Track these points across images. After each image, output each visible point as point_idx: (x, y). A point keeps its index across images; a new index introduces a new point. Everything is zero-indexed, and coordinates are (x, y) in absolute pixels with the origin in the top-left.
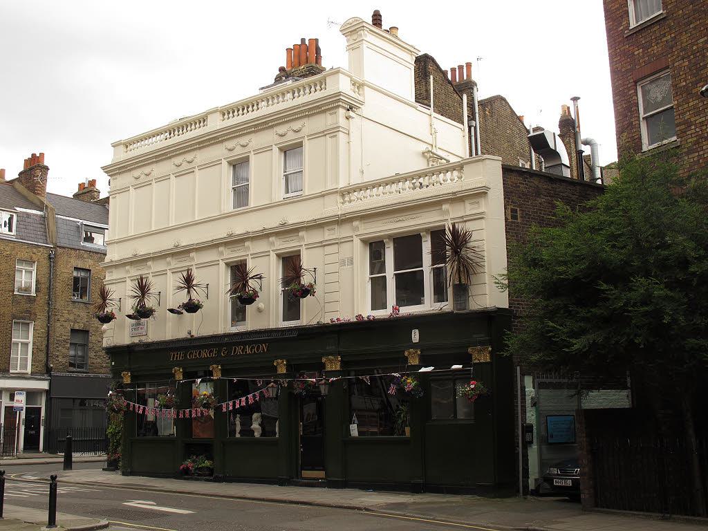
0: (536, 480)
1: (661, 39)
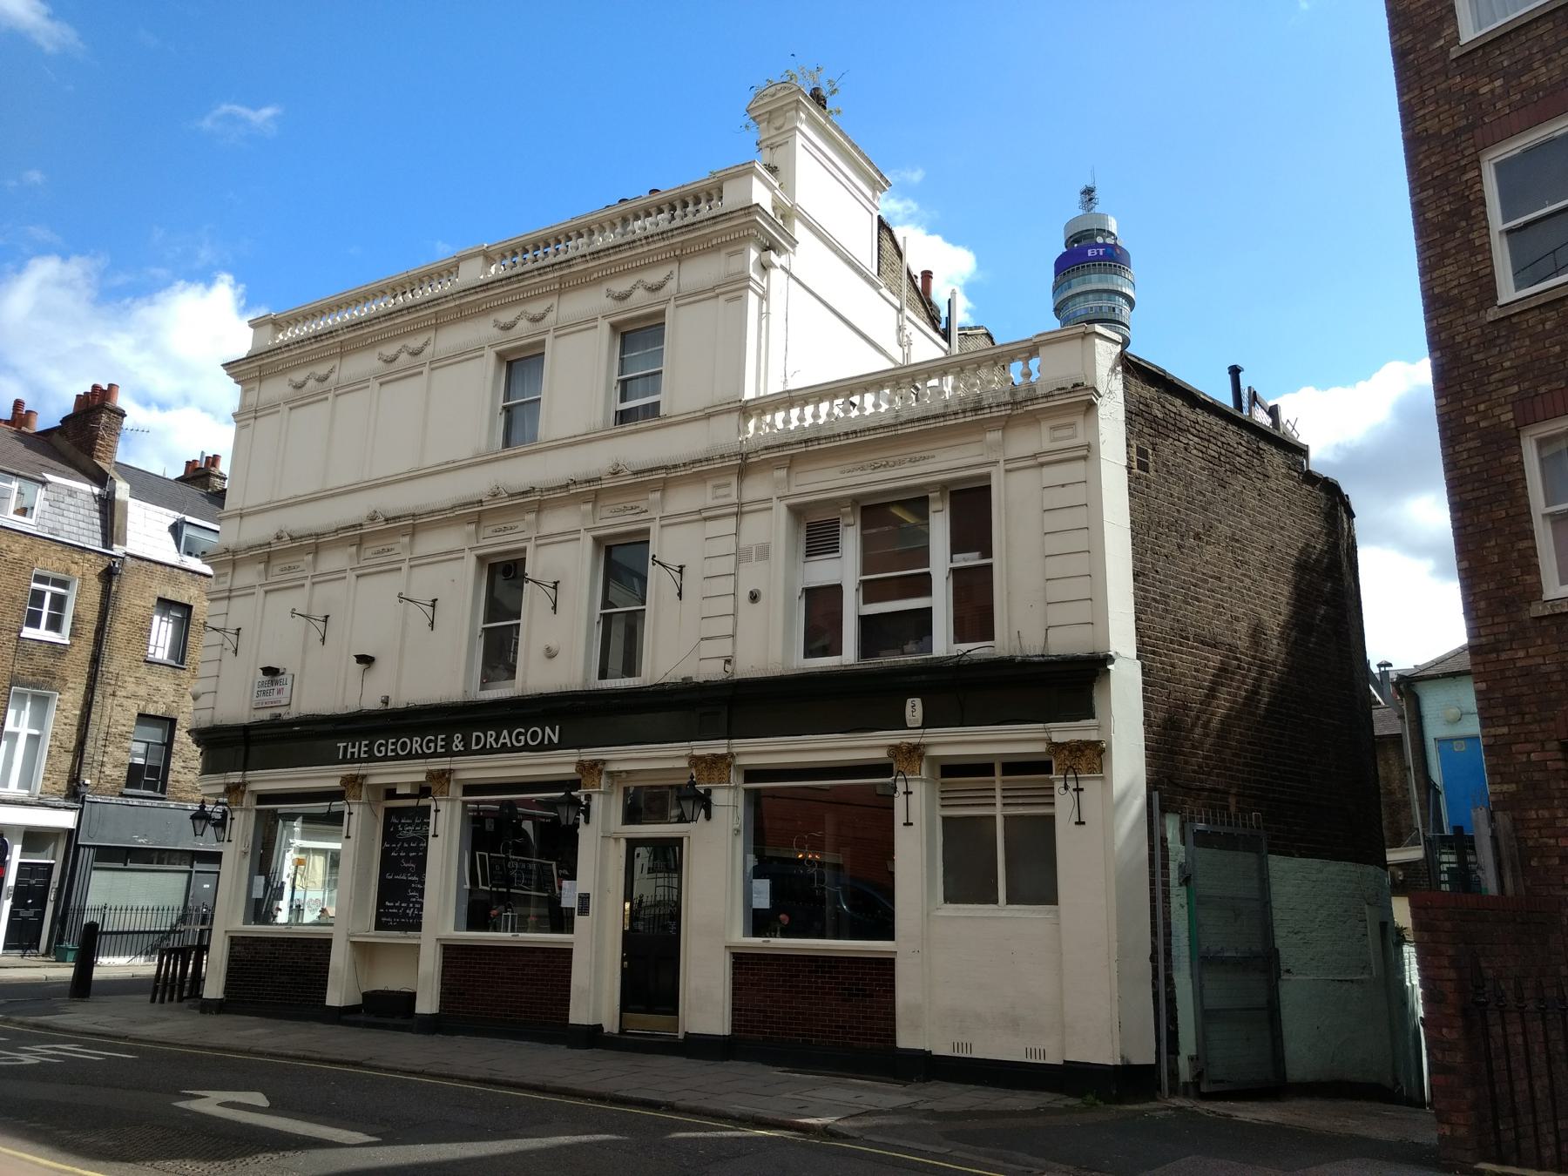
0: (1191, 1059)
1: (1559, 51)
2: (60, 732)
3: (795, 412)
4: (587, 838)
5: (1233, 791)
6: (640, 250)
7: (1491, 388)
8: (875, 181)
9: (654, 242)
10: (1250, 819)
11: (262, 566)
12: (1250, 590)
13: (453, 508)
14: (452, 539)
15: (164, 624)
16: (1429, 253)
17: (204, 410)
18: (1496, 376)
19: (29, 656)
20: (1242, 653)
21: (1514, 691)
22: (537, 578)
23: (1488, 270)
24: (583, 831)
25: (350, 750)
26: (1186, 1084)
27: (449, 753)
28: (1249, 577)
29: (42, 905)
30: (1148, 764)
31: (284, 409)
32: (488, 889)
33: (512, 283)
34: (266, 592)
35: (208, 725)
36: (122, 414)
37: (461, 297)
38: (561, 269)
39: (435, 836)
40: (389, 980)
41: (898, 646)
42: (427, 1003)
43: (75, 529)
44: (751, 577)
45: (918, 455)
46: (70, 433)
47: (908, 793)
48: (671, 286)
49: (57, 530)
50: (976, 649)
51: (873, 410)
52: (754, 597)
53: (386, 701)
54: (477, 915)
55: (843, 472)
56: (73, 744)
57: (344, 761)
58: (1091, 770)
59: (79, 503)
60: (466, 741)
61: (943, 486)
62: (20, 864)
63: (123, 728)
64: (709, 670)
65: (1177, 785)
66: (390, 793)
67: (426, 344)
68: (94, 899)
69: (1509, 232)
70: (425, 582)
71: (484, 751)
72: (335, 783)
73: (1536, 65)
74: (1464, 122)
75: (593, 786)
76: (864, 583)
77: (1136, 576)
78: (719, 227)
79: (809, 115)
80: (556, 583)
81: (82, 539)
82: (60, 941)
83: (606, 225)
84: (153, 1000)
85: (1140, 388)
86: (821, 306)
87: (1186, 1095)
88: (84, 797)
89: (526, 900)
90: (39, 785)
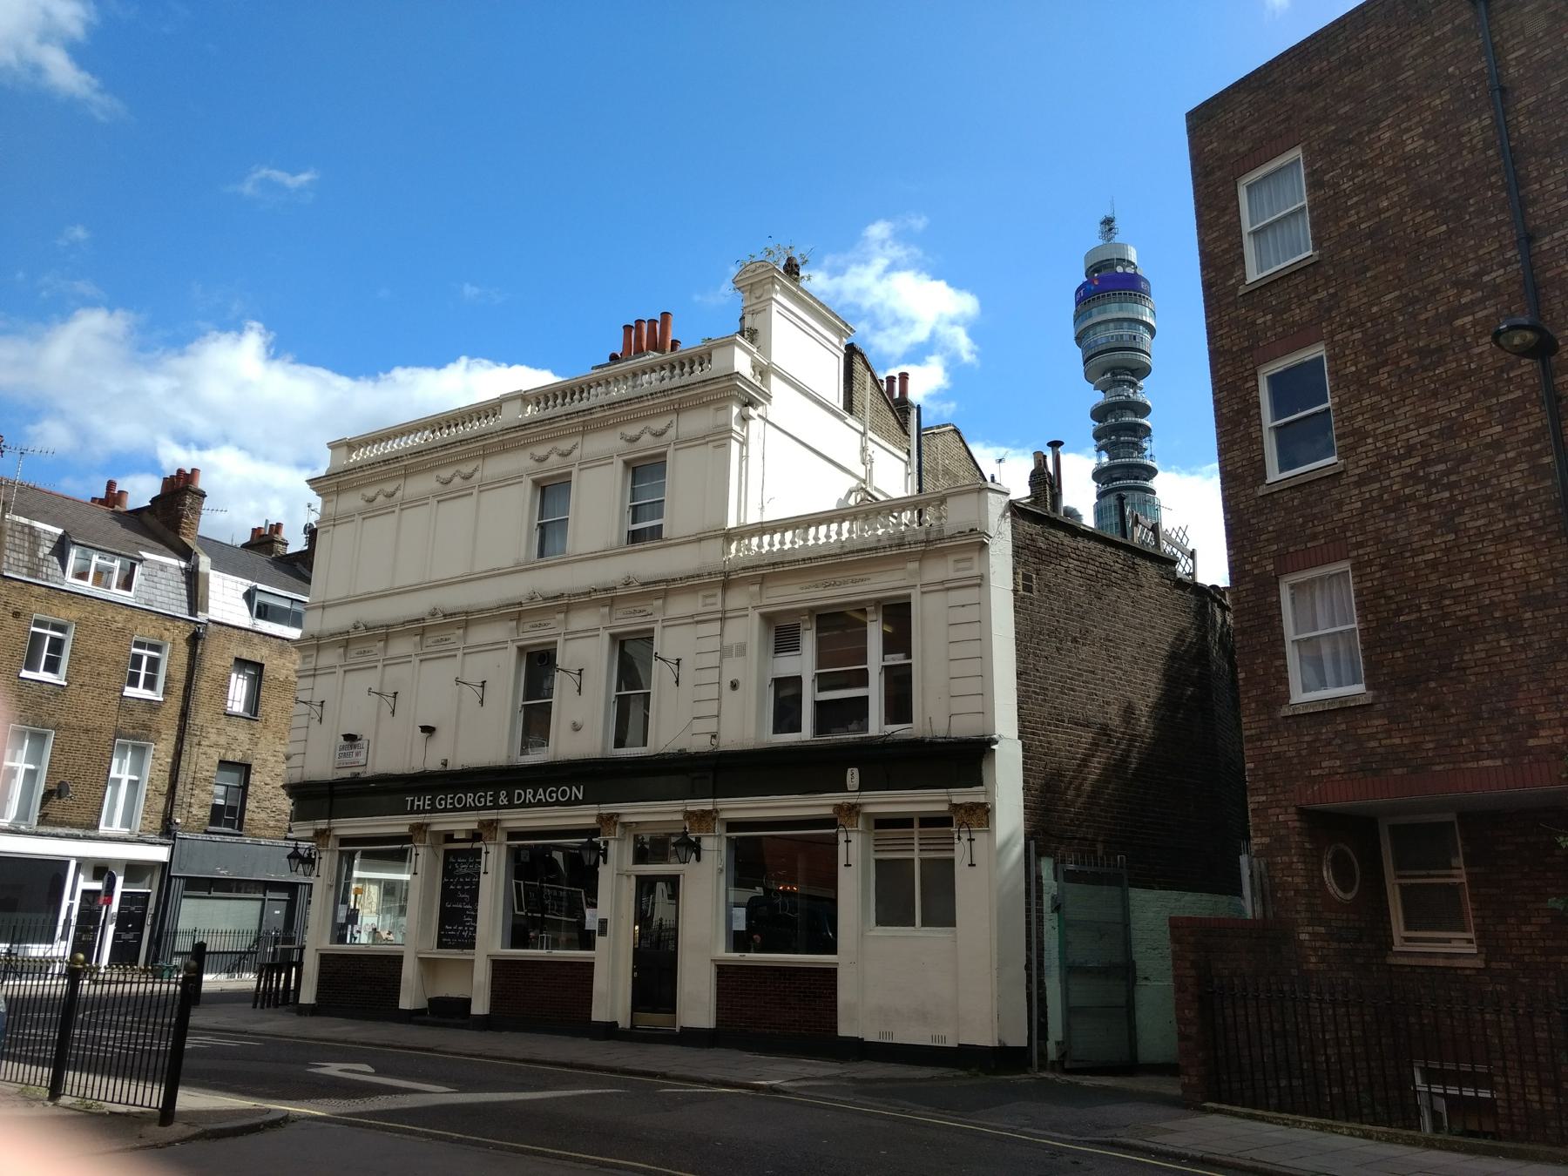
0: (1058, 1043)
2: (155, 777)
3: (766, 538)
4: (606, 874)
5: (1100, 839)
6: (646, 404)
7: (1261, 545)
8: (841, 330)
9: (658, 398)
10: (1116, 860)
11: (342, 650)
12: (1121, 679)
13: (499, 607)
14: (498, 632)
15: (240, 681)
16: (1224, 439)
17: (241, 448)
18: (1263, 537)
19: (130, 711)
20: (1112, 730)
21: (1270, 770)
22: (565, 668)
23: (1260, 457)
24: (602, 869)
25: (416, 803)
26: (1053, 1062)
27: (496, 806)
28: (1121, 669)
29: (140, 928)
30: (1026, 820)
31: (358, 519)
32: (523, 913)
33: (545, 425)
34: (345, 672)
35: (297, 781)
36: (203, 495)
37: (503, 435)
38: (584, 415)
39: (485, 873)
40: (450, 989)
41: (843, 725)
42: (480, 1007)
43: (166, 600)
44: (732, 670)
45: (858, 577)
46: (158, 512)
47: (848, 841)
48: (672, 432)
49: (151, 601)
50: (899, 730)
51: (825, 540)
52: (734, 686)
53: (445, 764)
54: (518, 935)
55: (802, 588)
56: (166, 788)
57: (412, 812)
58: (980, 825)
59: (169, 577)
60: (510, 797)
61: (877, 602)
62: (123, 893)
63: (207, 774)
64: (699, 743)
65: (1051, 835)
66: (449, 837)
67: (476, 470)
68: (184, 924)
69: (1277, 428)
70: (477, 666)
71: (523, 805)
72: (405, 830)
73: (1293, 307)
74: (1246, 344)
75: (610, 834)
76: (819, 675)
77: (1019, 675)
78: (708, 389)
79: (784, 287)
80: (581, 670)
81: (173, 608)
82: (156, 960)
83: (620, 378)
84: (255, 1007)
85: (1027, 527)
86: (794, 441)
87: (1053, 1070)
88: (175, 834)
89: (556, 925)
90: (138, 824)
